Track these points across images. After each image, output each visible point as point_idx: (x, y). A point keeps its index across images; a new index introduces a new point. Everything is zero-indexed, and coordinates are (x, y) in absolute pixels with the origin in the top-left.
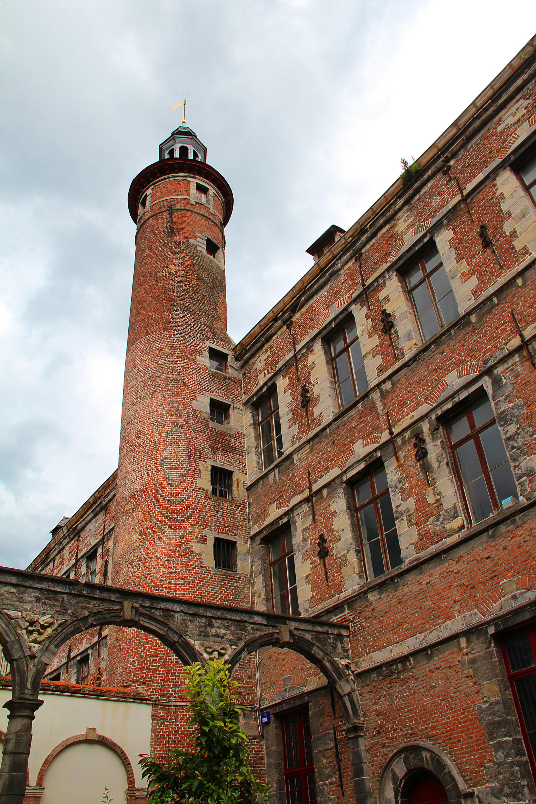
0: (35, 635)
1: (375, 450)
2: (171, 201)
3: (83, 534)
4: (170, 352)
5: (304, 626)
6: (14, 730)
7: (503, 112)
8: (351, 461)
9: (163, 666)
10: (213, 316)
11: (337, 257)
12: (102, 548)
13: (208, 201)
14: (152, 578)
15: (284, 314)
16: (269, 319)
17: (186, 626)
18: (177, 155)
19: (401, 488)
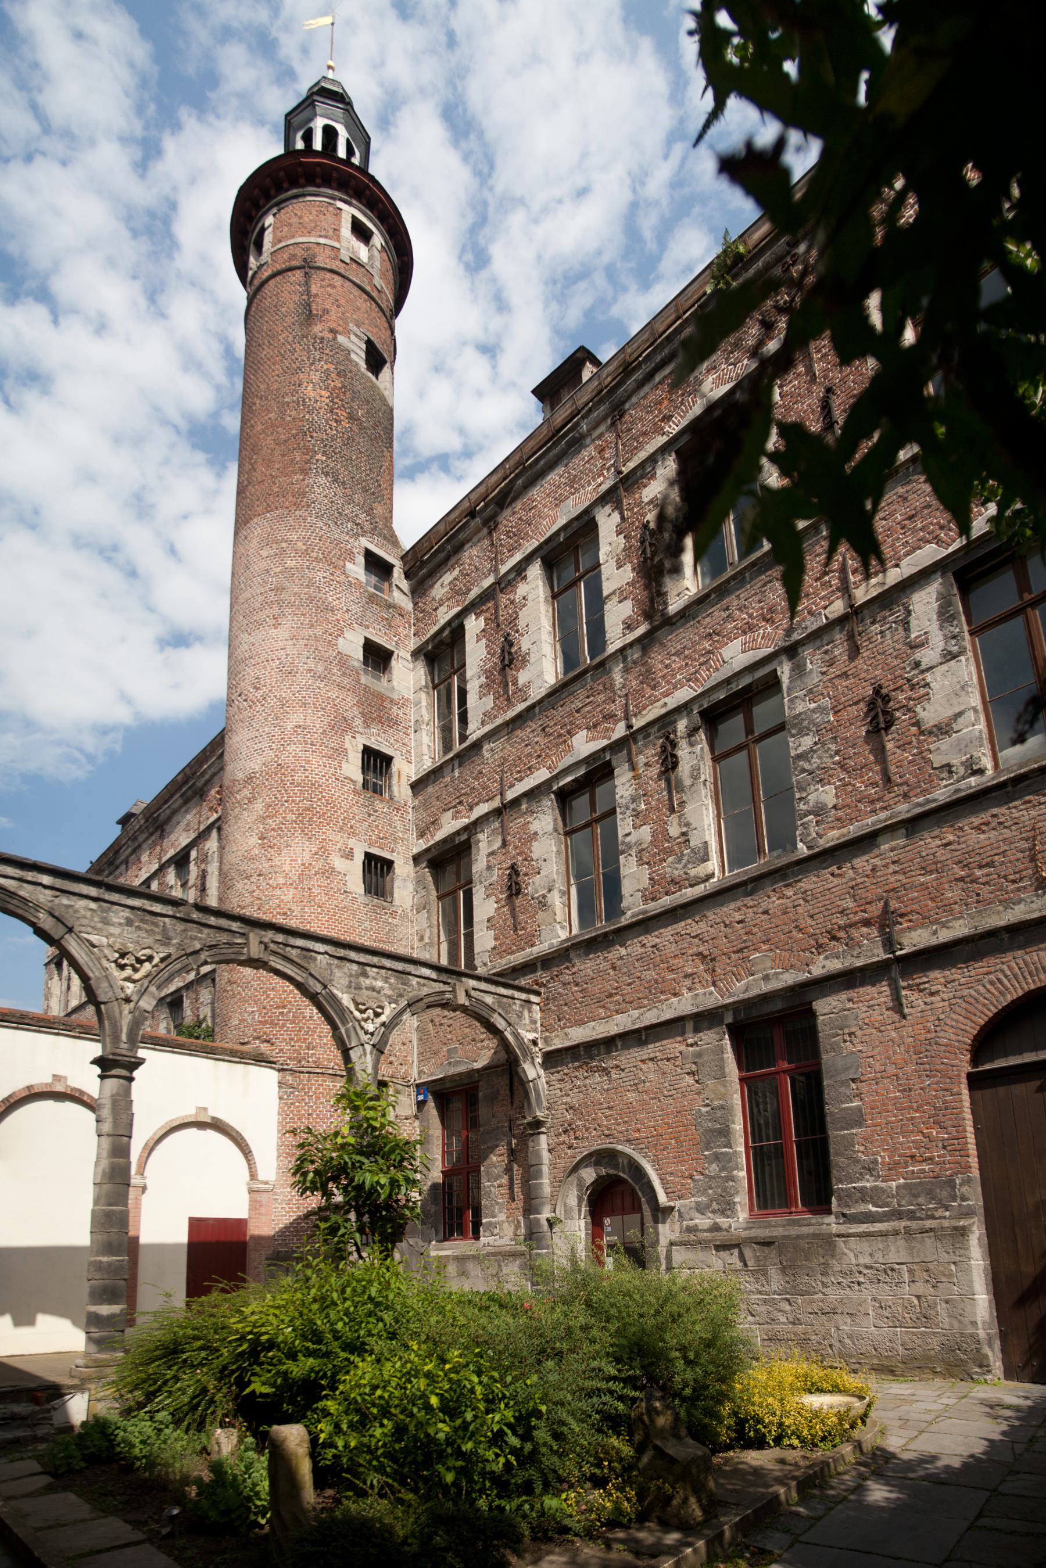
0: (129, 971)
1: (604, 750)
2: (307, 247)
4: (304, 547)
5: (483, 986)
6: (108, 1093)
8: (568, 760)
10: (373, 494)
13: (370, 258)
16: (462, 512)
18: (318, 145)
19: (634, 810)
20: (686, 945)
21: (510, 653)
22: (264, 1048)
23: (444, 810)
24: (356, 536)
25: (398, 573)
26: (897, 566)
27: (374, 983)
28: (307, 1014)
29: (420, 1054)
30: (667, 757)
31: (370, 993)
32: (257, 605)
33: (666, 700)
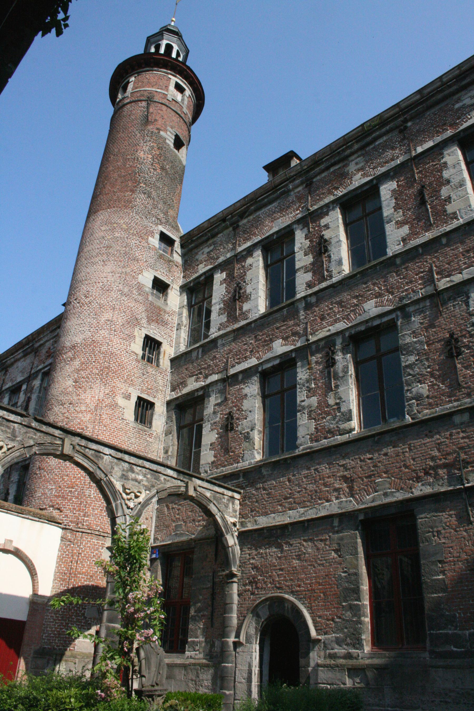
1: (291, 351)
2: (150, 92)
3: (10, 370)
4: (126, 228)
7: (463, 93)
8: (269, 355)
9: (77, 498)
10: (169, 205)
11: (291, 179)
12: (27, 385)
13: (183, 100)
14: (79, 421)
15: (232, 217)
17: (113, 468)
18: (162, 51)
19: (307, 387)
20: (336, 470)
21: (239, 293)
22: (55, 513)
23: (190, 376)
24: (157, 224)
25: (177, 245)
26: (461, 273)
27: (137, 477)
28: (87, 493)
29: (156, 527)
30: (329, 359)
31: (134, 483)
32: (94, 254)
33: (330, 328)
